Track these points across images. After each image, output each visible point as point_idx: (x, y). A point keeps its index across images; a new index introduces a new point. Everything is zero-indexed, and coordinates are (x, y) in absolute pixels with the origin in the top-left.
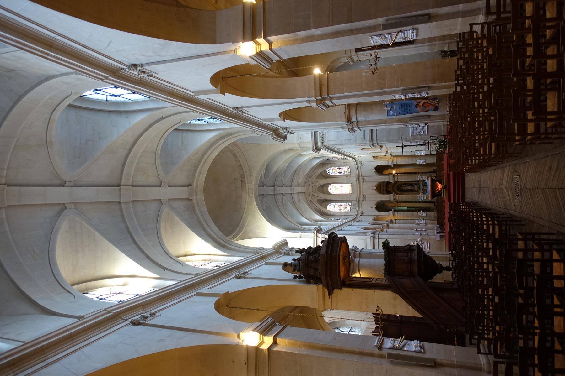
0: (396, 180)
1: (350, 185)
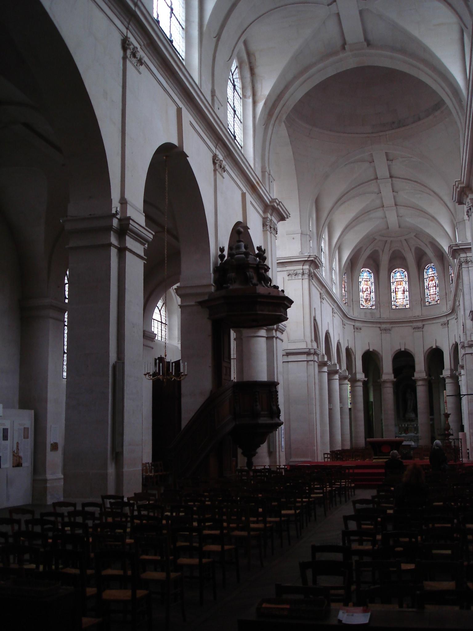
1: (408, 306)
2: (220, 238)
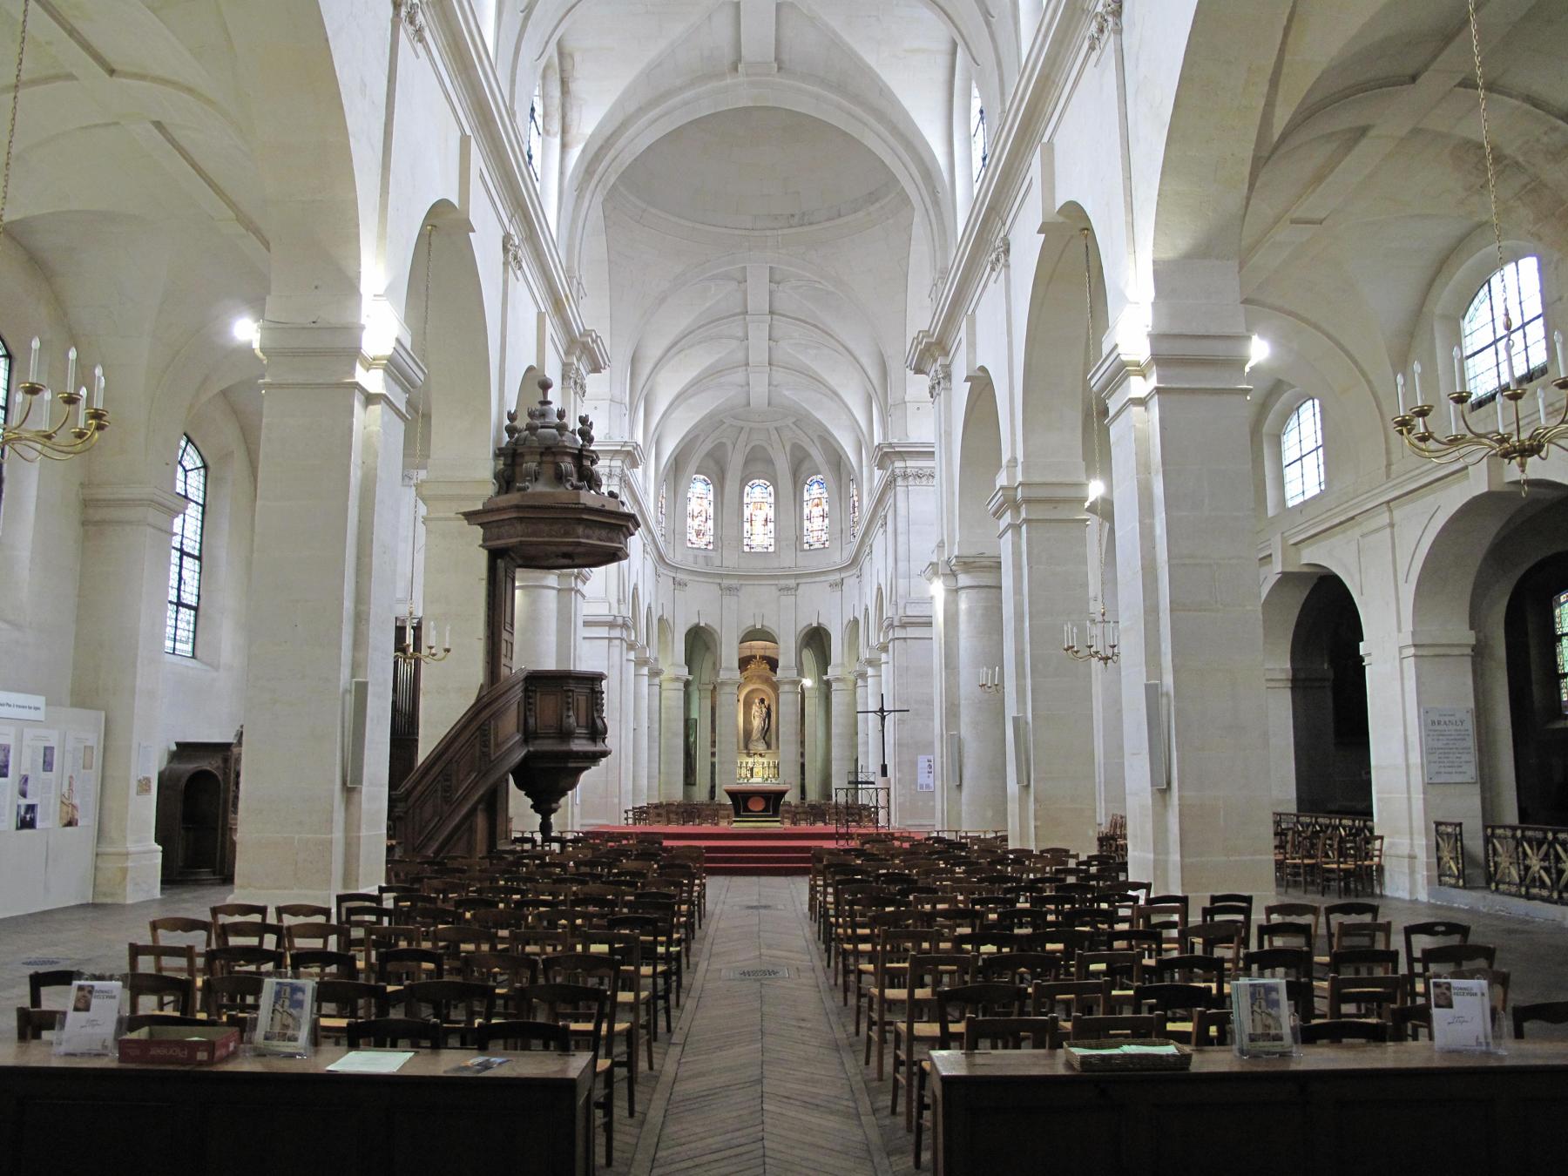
0: (785, 688)
1: (771, 549)
2: (506, 396)
